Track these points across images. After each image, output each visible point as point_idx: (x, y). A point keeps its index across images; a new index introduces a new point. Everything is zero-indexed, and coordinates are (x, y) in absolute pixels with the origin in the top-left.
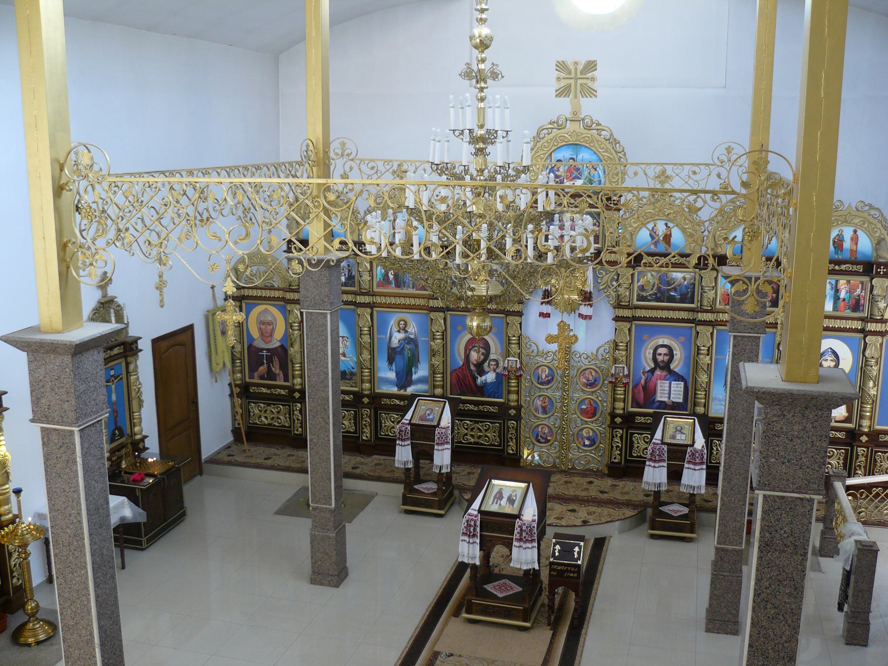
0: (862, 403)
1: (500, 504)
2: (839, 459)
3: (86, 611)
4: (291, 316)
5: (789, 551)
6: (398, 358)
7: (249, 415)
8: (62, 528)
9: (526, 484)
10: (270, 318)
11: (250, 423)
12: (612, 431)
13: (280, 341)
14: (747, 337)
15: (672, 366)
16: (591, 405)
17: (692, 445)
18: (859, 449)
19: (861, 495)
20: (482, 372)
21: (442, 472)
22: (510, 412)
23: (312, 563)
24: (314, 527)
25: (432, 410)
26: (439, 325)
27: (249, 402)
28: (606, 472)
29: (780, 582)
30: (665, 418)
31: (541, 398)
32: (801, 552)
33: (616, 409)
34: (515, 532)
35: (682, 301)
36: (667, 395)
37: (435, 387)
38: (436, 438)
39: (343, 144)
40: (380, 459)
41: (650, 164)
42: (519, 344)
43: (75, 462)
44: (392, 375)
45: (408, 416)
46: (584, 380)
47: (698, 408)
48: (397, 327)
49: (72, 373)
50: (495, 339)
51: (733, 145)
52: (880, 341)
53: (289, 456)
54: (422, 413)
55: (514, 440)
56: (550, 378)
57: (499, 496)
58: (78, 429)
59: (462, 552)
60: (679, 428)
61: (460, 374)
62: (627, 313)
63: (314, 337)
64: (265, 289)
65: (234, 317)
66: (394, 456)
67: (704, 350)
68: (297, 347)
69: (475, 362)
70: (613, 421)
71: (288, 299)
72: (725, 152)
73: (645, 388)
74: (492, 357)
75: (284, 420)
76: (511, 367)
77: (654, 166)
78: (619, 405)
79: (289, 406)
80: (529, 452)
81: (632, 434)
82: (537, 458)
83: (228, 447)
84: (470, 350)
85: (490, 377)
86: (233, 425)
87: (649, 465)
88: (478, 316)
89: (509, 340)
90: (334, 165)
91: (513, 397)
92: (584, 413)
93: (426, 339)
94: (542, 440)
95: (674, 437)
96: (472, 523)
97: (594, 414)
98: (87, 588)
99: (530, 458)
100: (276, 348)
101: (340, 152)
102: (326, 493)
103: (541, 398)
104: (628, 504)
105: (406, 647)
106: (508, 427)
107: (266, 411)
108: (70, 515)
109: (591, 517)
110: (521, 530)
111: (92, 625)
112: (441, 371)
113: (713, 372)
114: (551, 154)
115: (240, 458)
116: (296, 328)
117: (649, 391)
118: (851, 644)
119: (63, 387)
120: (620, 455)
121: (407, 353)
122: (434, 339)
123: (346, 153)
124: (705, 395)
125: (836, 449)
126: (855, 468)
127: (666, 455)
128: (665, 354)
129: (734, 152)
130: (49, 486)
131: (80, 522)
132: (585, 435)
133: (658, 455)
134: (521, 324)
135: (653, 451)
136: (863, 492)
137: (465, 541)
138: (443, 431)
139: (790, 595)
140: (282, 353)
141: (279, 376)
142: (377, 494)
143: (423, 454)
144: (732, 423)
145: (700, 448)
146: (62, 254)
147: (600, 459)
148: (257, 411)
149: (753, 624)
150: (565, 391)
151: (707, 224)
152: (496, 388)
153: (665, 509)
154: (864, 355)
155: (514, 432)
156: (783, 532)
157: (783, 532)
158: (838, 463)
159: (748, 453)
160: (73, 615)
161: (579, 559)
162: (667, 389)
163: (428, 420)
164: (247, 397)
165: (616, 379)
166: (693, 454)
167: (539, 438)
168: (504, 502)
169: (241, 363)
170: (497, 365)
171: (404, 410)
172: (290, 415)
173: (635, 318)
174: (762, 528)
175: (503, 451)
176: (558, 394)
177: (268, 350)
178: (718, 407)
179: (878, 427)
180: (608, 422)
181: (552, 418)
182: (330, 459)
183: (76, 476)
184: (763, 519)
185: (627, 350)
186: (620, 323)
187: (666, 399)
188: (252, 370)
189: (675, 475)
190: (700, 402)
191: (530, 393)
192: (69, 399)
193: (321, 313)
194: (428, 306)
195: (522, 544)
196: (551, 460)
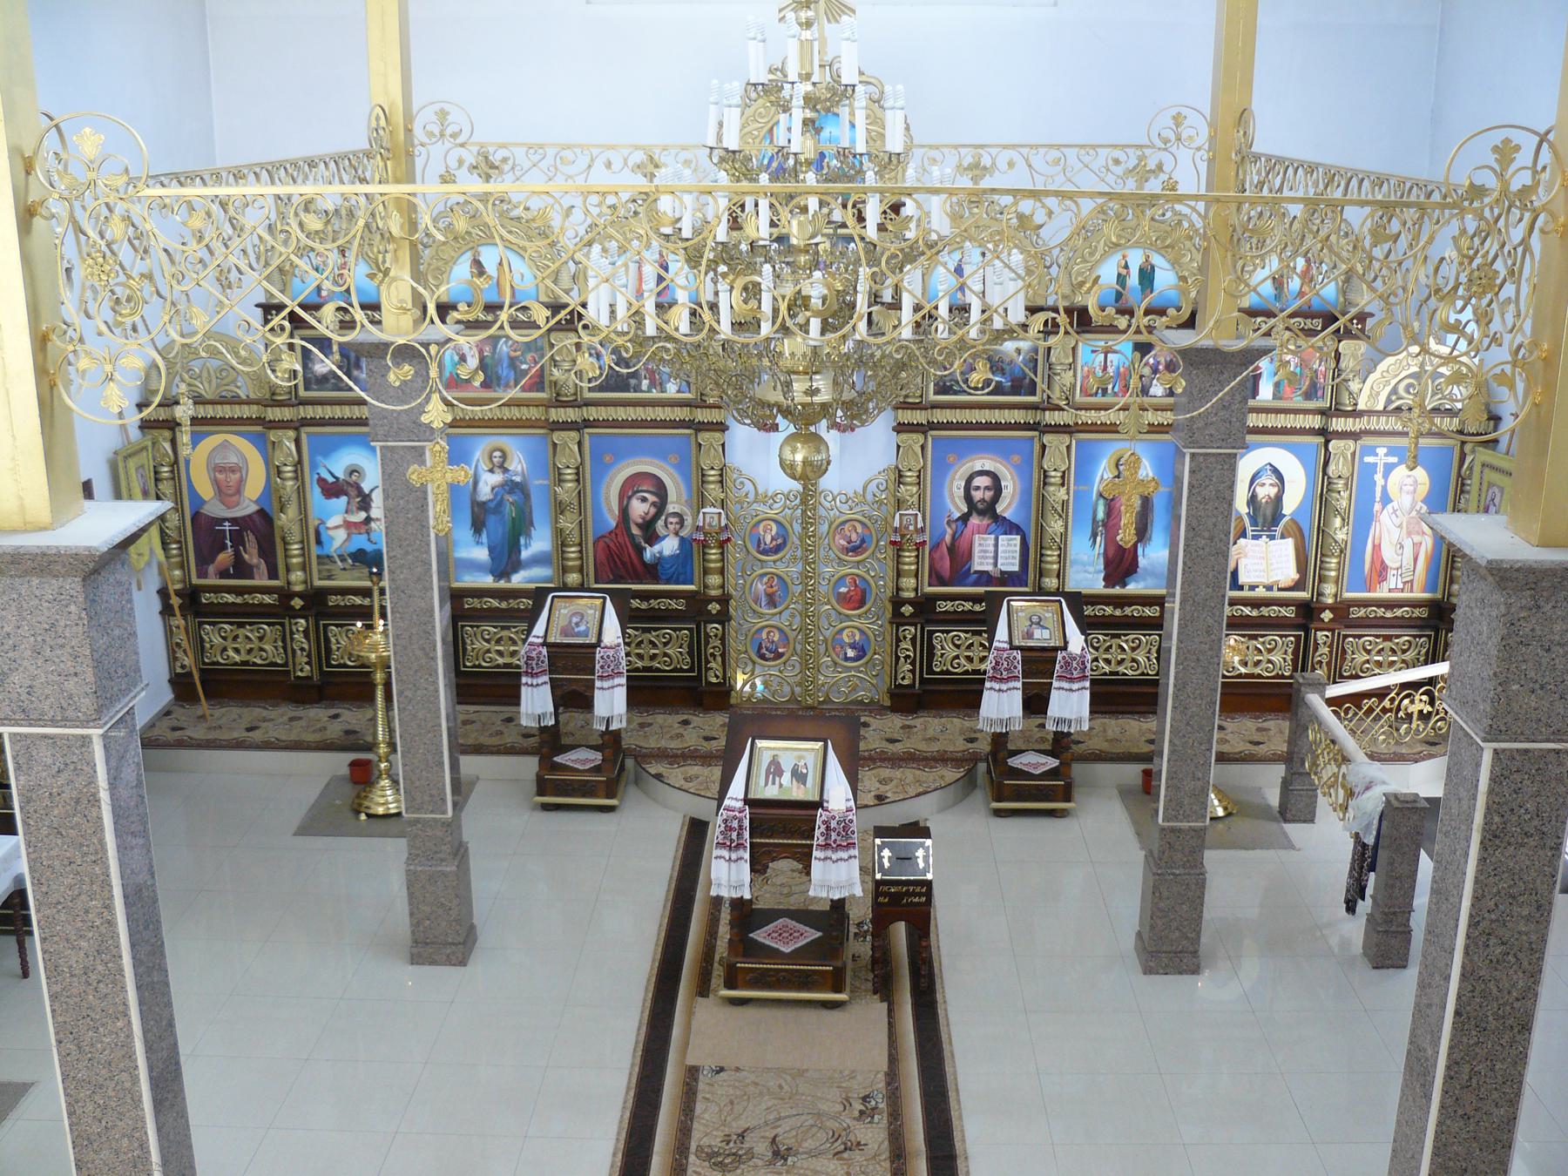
0: (1322, 555)
1: (781, 785)
2: (1286, 653)
3: (129, 1101)
4: (277, 452)
5: (1533, 843)
6: (492, 520)
7: (203, 647)
8: (67, 940)
9: (821, 743)
10: (233, 459)
11: (204, 663)
12: (897, 630)
13: (256, 502)
14: (1214, 454)
15: (999, 509)
16: (856, 586)
17: (1065, 648)
18: (1319, 634)
19: (1346, 713)
20: (653, 538)
21: (611, 728)
22: (710, 607)
23: (412, 925)
24: (412, 858)
25: (582, 616)
26: (568, 459)
27: (201, 624)
28: (887, 703)
29: (1514, 898)
30: (1009, 601)
31: (765, 579)
32: (1550, 843)
33: (902, 590)
34: (817, 833)
35: (1015, 390)
36: (992, 561)
37: (565, 570)
38: (597, 667)
39: (443, 115)
40: (467, 713)
41: (1037, 146)
42: (721, 482)
43: (95, 801)
44: (481, 554)
45: (539, 629)
46: (843, 542)
47: (1047, 580)
48: (488, 462)
49: (83, 614)
50: (676, 475)
51: (1185, 111)
52: (1352, 449)
53: (291, 719)
54: (563, 623)
55: (719, 659)
56: (780, 541)
57: (775, 769)
58: (101, 731)
59: (718, 879)
60: (1035, 619)
61: (612, 545)
62: (919, 417)
63: (399, 494)
64: (221, 403)
65: (449, 475)
66: (518, 704)
67: (1055, 477)
68: (292, 511)
69: (640, 521)
70: (897, 613)
71: (270, 421)
72: (1171, 123)
73: (952, 549)
74: (671, 508)
75: (271, 652)
76: (710, 525)
77: (1044, 150)
78: (908, 582)
79: (282, 625)
80: (746, 677)
81: (931, 633)
82: (760, 687)
83: (167, 713)
84: (630, 498)
85: (668, 546)
86: (171, 668)
87: (991, 689)
88: (804, 443)
89: (703, 475)
90: (424, 156)
91: (714, 580)
92: (844, 600)
93: (545, 482)
94: (768, 655)
95: (1029, 635)
96: (735, 824)
97: (862, 603)
98: (131, 1056)
99: (747, 688)
100: (249, 516)
101: (436, 130)
102: (434, 792)
103: (765, 579)
104: (943, 759)
105: (633, 1065)
106: (707, 636)
107: (235, 638)
108: (87, 912)
109: (887, 788)
110: (828, 828)
111: (144, 1127)
112: (577, 541)
113: (1070, 514)
114: (772, 129)
115: (199, 733)
116: (290, 475)
117: (959, 555)
118: (1382, 967)
119: (62, 646)
120: (913, 671)
121: (509, 511)
122: (560, 481)
123: (449, 131)
124: (1059, 556)
125: (1281, 636)
126: (1313, 666)
127: (1020, 667)
128: (987, 488)
129: (1186, 123)
130: (33, 856)
131: (111, 923)
132: (847, 640)
133: (1006, 669)
134: (723, 445)
135: (997, 663)
136: (1349, 708)
137: (720, 857)
138: (611, 652)
139: (1528, 918)
140: (262, 526)
141: (258, 568)
142: (478, 778)
143: (573, 698)
144: (1188, 608)
145: (1079, 652)
146: (40, 357)
147: (874, 682)
148: (217, 640)
149: (1464, 976)
150: (809, 564)
151: (1056, 252)
152: (682, 565)
153: (1015, 762)
154: (1325, 473)
155: (717, 643)
156: (1523, 811)
157: (1523, 811)
158: (1284, 659)
159: (1216, 660)
160: (98, 1113)
161: (926, 871)
162: (992, 548)
163: (578, 635)
164: (197, 614)
165: (903, 536)
166: (1067, 664)
167: (764, 651)
168: (786, 778)
169: (180, 548)
170: (682, 522)
171: (531, 617)
172: (284, 641)
173: (932, 426)
174: (1488, 808)
175: (699, 678)
176: (795, 569)
177: (234, 521)
178: (1082, 575)
179: (1348, 595)
180: (889, 615)
181: (785, 615)
182: (440, 725)
183: (99, 828)
184: (1491, 792)
185: (919, 484)
186: (904, 436)
187: (989, 568)
188: (204, 559)
189: (1036, 703)
190: (1050, 570)
191: (743, 571)
192: (79, 669)
193: (413, 447)
194: (547, 420)
195: (829, 853)
196: (787, 689)
